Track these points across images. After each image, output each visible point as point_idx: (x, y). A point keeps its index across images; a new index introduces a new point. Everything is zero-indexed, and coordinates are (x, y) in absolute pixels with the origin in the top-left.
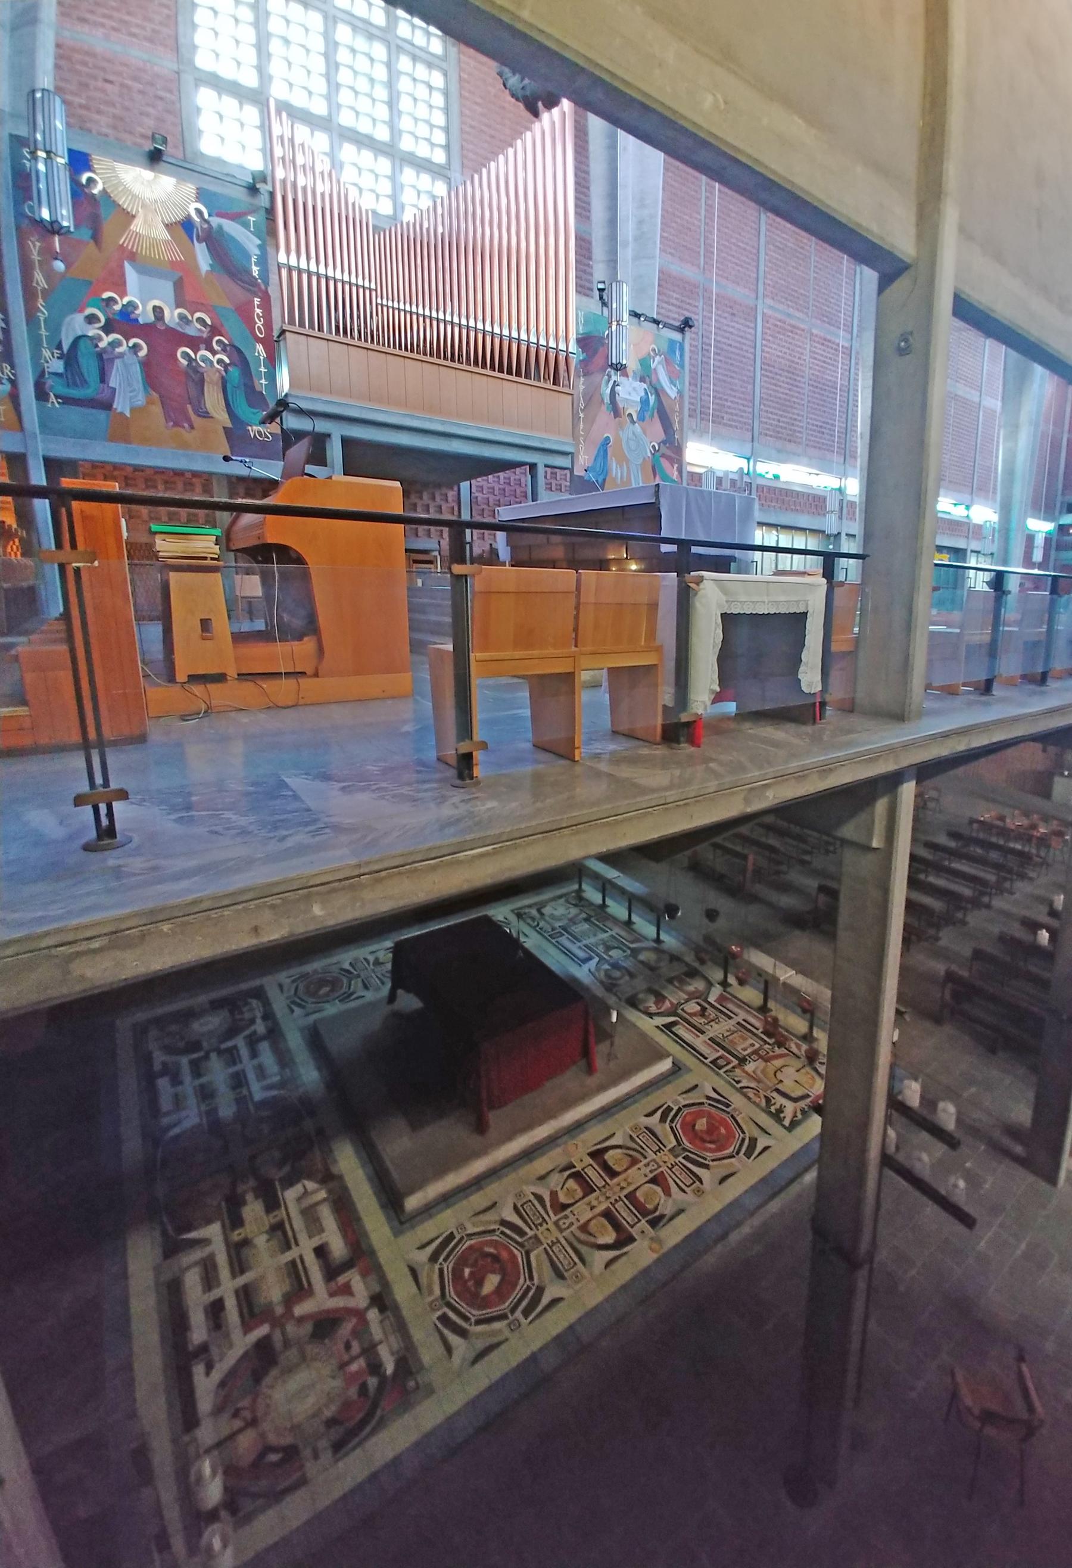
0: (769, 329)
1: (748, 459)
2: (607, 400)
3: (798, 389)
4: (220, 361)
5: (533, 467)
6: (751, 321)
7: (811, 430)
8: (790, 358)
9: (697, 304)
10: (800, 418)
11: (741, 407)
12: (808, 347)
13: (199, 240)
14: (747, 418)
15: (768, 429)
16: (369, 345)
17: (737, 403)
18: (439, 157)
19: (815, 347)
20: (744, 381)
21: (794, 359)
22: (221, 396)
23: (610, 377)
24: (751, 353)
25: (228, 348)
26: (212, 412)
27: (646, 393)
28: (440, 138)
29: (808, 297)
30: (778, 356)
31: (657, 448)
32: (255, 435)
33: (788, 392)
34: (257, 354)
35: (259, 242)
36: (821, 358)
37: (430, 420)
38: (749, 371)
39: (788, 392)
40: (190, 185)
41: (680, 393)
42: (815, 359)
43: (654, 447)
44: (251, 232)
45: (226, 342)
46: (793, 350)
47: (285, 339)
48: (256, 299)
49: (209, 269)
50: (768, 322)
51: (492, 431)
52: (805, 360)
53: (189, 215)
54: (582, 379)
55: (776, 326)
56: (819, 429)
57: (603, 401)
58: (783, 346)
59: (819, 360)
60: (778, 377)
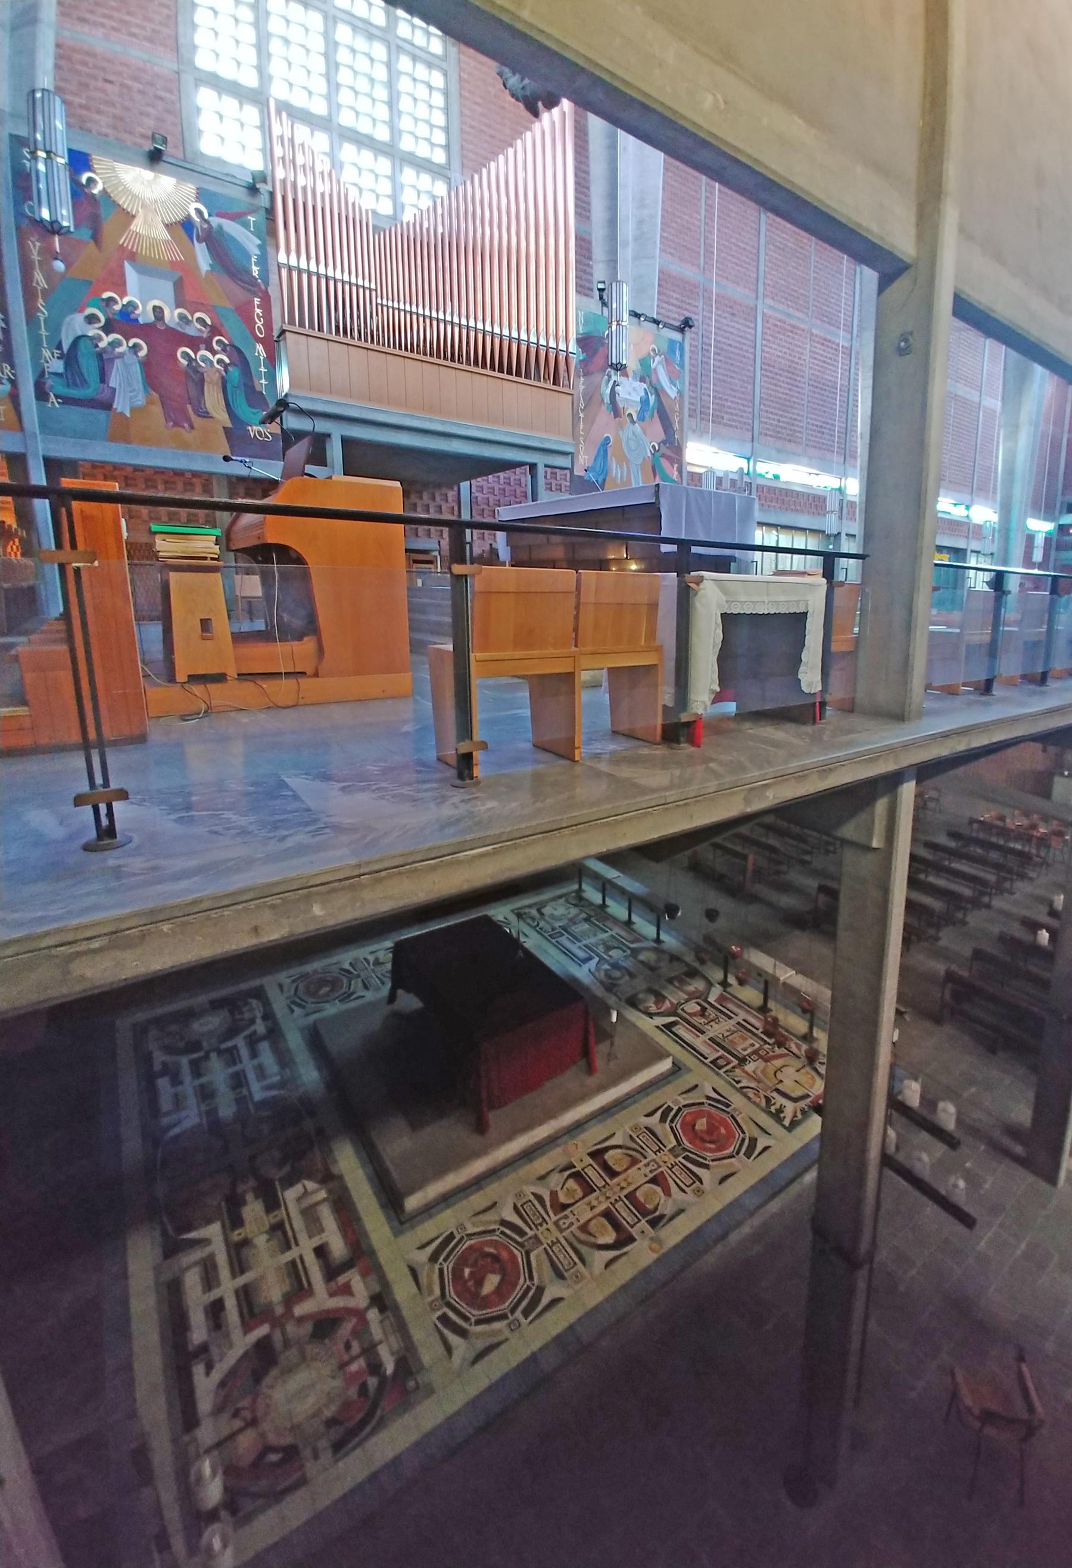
0: (769, 329)
1: (748, 459)
2: (607, 400)
3: (798, 389)
4: (220, 361)
5: (533, 467)
6: (751, 321)
7: (811, 430)
8: (790, 358)
9: (697, 304)
10: (800, 418)
12: (808, 347)
13: (199, 240)
14: (747, 418)
16: (369, 345)
17: (737, 403)
18: (439, 157)
19: (815, 347)
20: (744, 381)
21: (794, 359)
22: (221, 396)
23: (610, 377)
24: (751, 353)
25: (228, 348)
26: (212, 412)
27: (646, 393)
28: (440, 138)
29: (808, 297)
30: (778, 356)
31: (657, 448)
32: (255, 435)
33: (788, 392)
34: (257, 354)
35: (259, 242)
37: (430, 420)
38: (749, 371)
39: (788, 392)
40: (190, 185)
41: (680, 393)
42: (815, 359)
43: (654, 447)
44: (251, 232)
45: (226, 342)
46: (793, 350)
47: (285, 339)
48: (256, 299)
49: (209, 269)
50: (768, 322)
51: (492, 431)
52: (805, 360)
53: (189, 215)
54: (582, 379)
55: (776, 326)
56: (819, 429)
57: (603, 401)
58: (783, 346)
59: (819, 360)
60: (778, 377)
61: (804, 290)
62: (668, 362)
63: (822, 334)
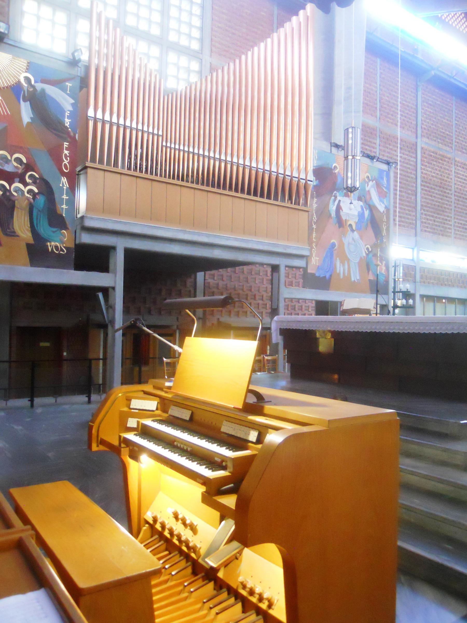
0: (426, 158)
1: (413, 249)
2: (333, 214)
3: (448, 199)
4: (30, 191)
5: (275, 268)
6: (413, 153)
7: (457, 227)
8: (440, 177)
9: (375, 141)
10: (449, 219)
11: (407, 212)
12: (453, 170)
13: (25, 101)
14: (412, 220)
15: (427, 227)
16: (153, 177)
17: (405, 209)
18: (195, 46)
19: (459, 170)
20: (409, 194)
21: (443, 178)
22: (27, 219)
23: (336, 197)
24: (414, 174)
25: (38, 181)
26: (19, 232)
27: (362, 209)
28: (196, 34)
29: (452, 137)
30: (433, 176)
31: (370, 250)
32: (52, 249)
33: (440, 200)
34: (61, 185)
35: (73, 101)
36: (462, 177)
37: (199, 234)
38: (413, 186)
39: (440, 200)
40: (22, 60)
41: (387, 209)
42: (459, 178)
43: (368, 249)
44: (67, 94)
45: (37, 176)
46: (443, 172)
47: (86, 173)
48: (65, 143)
49: (30, 120)
50: (425, 153)
51: (248, 241)
52: (451, 179)
53: (19, 82)
54: (315, 200)
55: (431, 156)
56: (462, 226)
57: (330, 216)
58: (436, 170)
59: (462, 179)
60: (433, 191)
61: (449, 132)
62: (378, 185)
63: (462, 161)
